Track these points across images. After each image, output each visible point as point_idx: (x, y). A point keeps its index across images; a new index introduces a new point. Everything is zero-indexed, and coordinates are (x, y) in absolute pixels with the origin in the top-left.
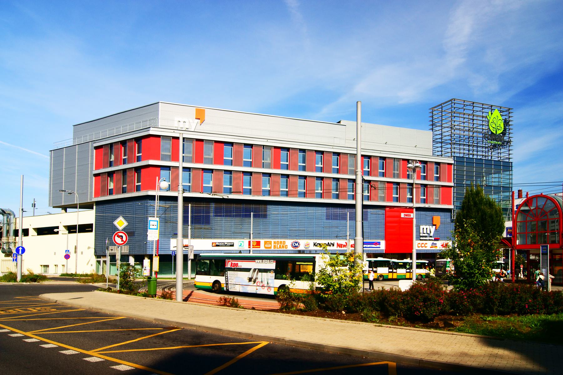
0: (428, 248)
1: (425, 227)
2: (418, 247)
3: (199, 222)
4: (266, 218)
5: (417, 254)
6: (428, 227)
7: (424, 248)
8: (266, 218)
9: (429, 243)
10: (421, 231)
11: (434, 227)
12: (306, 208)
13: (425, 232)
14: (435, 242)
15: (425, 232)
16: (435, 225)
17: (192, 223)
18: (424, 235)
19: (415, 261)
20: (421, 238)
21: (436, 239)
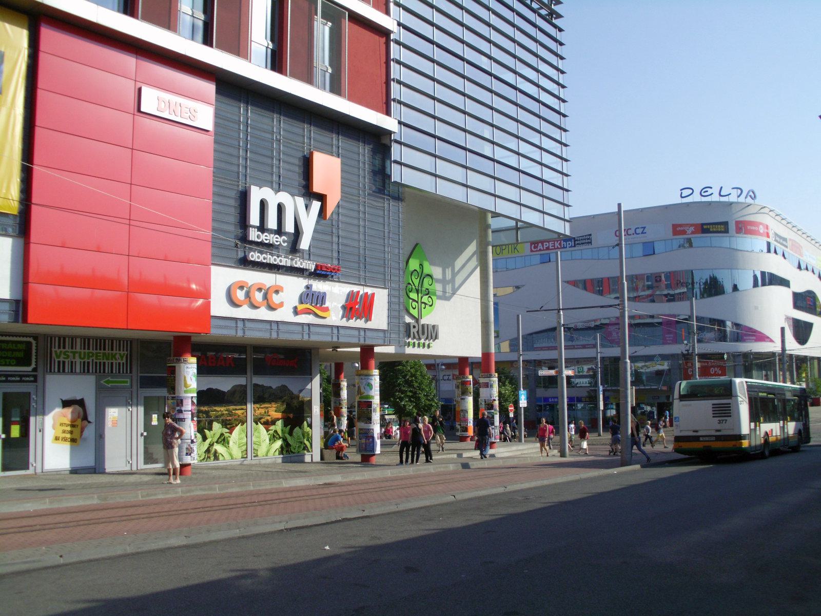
0: (285, 314)
1: (274, 198)
2: (233, 303)
3: (632, 346)
4: (784, 328)
5: (495, 362)
6: (284, 197)
7: (263, 314)
8: (784, 328)
9: (292, 288)
10: (254, 219)
11: (316, 205)
12: (505, 167)
13: (272, 223)
14: (319, 286)
15: (272, 223)
16: (322, 198)
17: (629, 346)
18: (265, 238)
19: (110, 361)
20: (254, 256)
21: (320, 274)
